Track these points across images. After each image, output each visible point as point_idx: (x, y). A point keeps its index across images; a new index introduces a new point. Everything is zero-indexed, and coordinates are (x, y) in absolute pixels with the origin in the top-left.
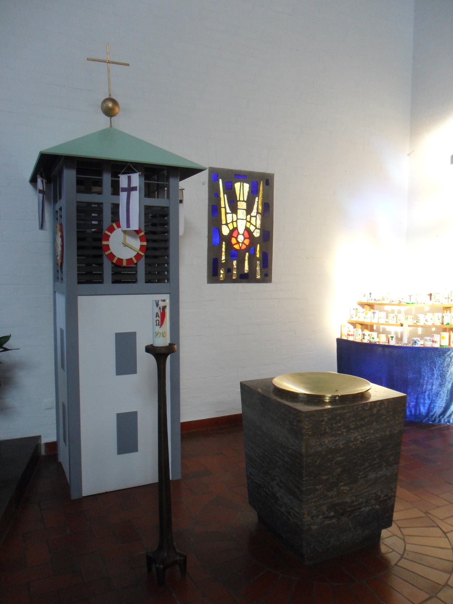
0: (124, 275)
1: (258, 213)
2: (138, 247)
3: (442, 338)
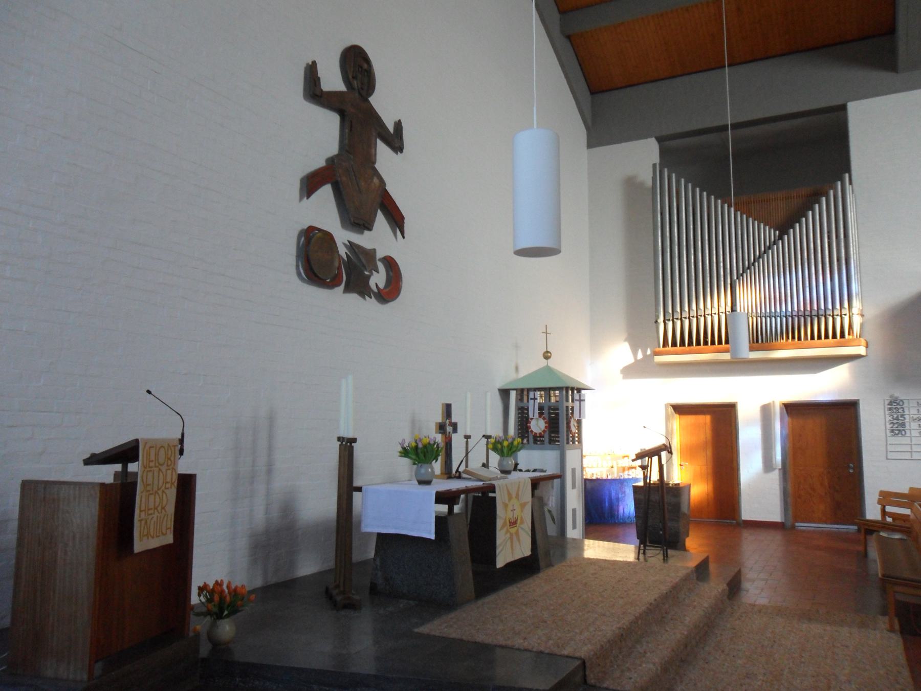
0: (538, 440)
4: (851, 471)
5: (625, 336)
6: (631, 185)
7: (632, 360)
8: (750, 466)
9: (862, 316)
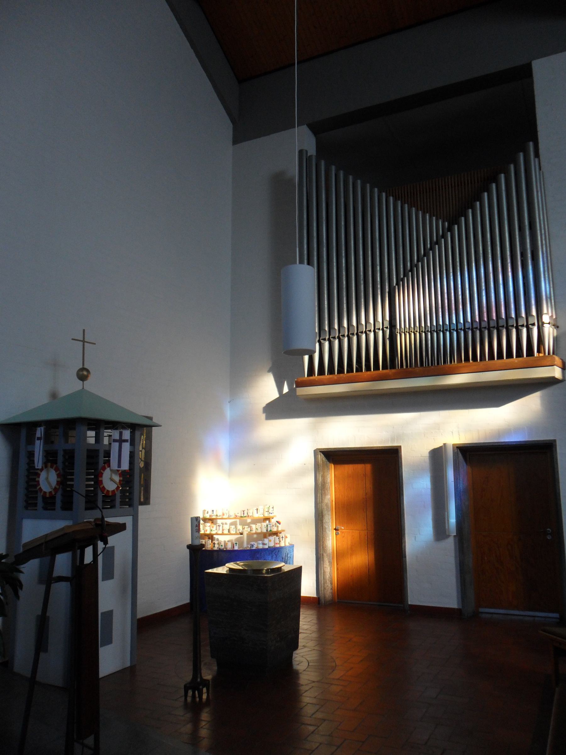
0: (49, 502)
1: (143, 448)
2: (118, 481)
3: (270, 541)
4: (549, 537)
5: (269, 365)
6: (279, 182)
7: (276, 395)
8: (419, 533)
9: (556, 326)
